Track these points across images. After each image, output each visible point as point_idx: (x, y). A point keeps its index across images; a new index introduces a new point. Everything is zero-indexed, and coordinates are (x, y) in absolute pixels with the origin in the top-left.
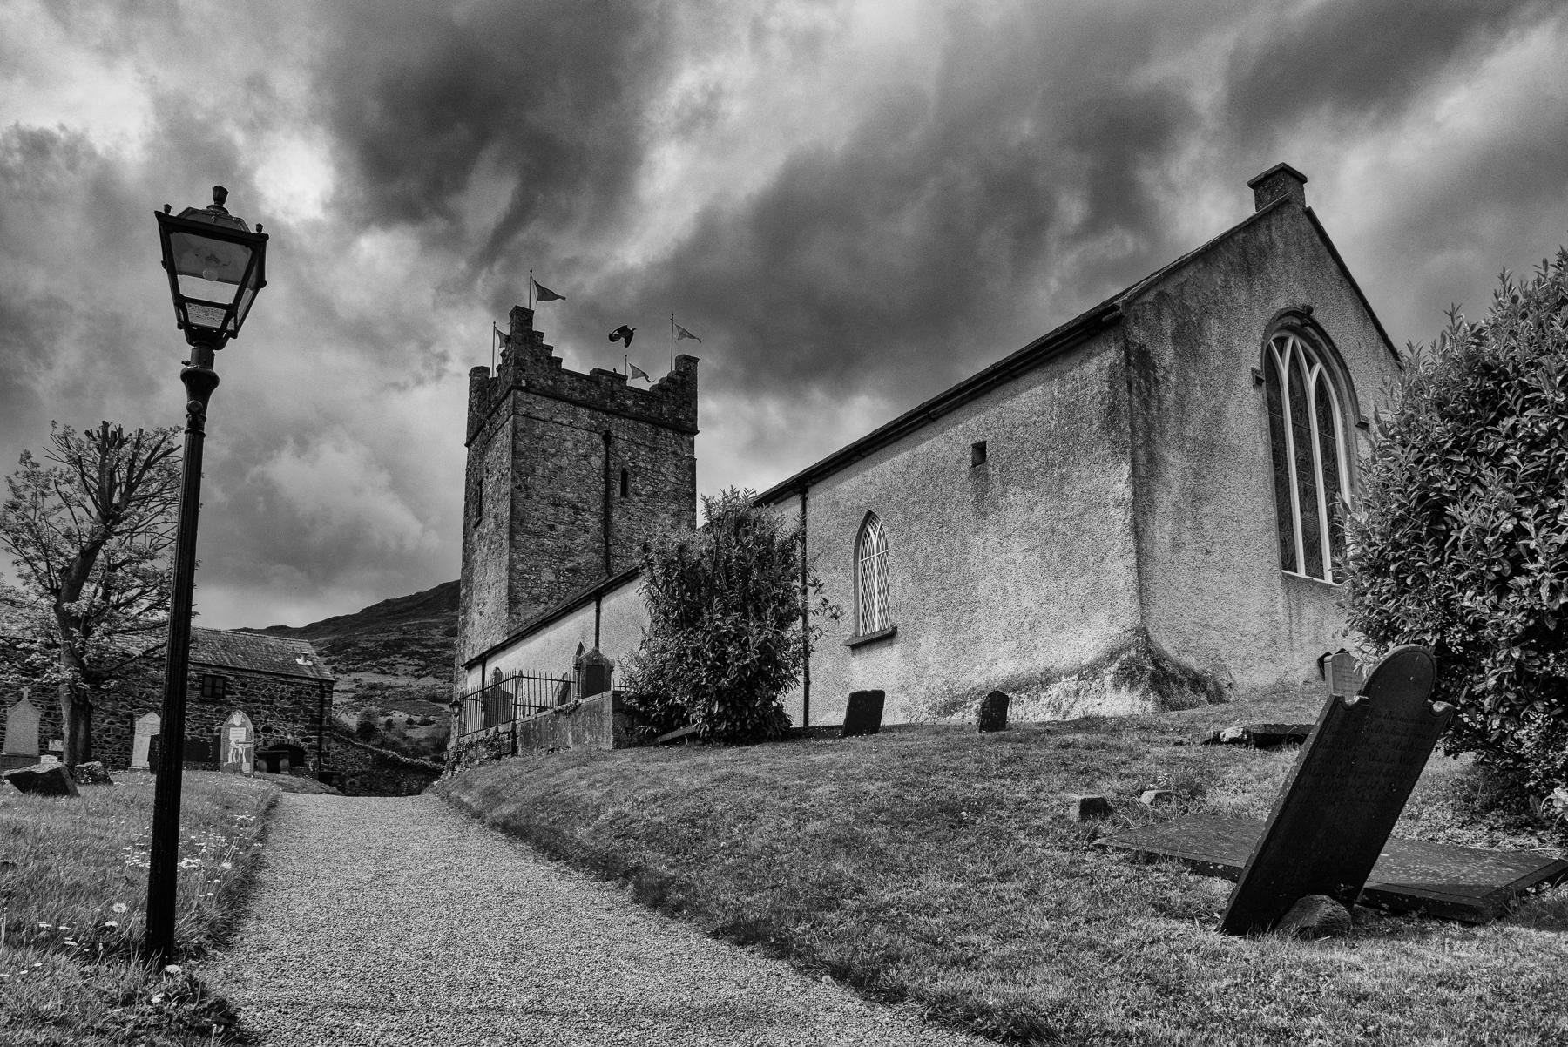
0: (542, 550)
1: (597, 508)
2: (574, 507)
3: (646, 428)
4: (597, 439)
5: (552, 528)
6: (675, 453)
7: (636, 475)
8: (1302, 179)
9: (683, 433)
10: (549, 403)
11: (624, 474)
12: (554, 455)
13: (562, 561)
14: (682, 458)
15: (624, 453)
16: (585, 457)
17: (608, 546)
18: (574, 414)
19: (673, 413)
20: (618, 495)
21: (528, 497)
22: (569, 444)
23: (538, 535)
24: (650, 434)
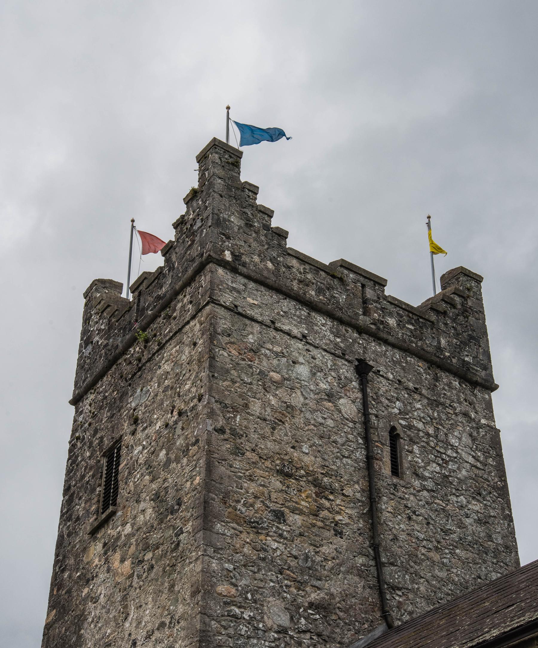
0: (263, 558)
1: (355, 490)
2: (316, 483)
3: (421, 367)
4: (347, 371)
5: (279, 516)
6: (466, 415)
7: (412, 441)
8: (478, 279)
9: (474, 384)
10: (270, 297)
11: (394, 436)
12: (278, 384)
13: (300, 585)
14: (479, 426)
15: (391, 408)
16: (330, 396)
17: (379, 565)
18: (310, 324)
19: (457, 350)
20: (387, 470)
21: (238, 451)
22: (303, 371)
23: (255, 526)
24: (427, 377)
